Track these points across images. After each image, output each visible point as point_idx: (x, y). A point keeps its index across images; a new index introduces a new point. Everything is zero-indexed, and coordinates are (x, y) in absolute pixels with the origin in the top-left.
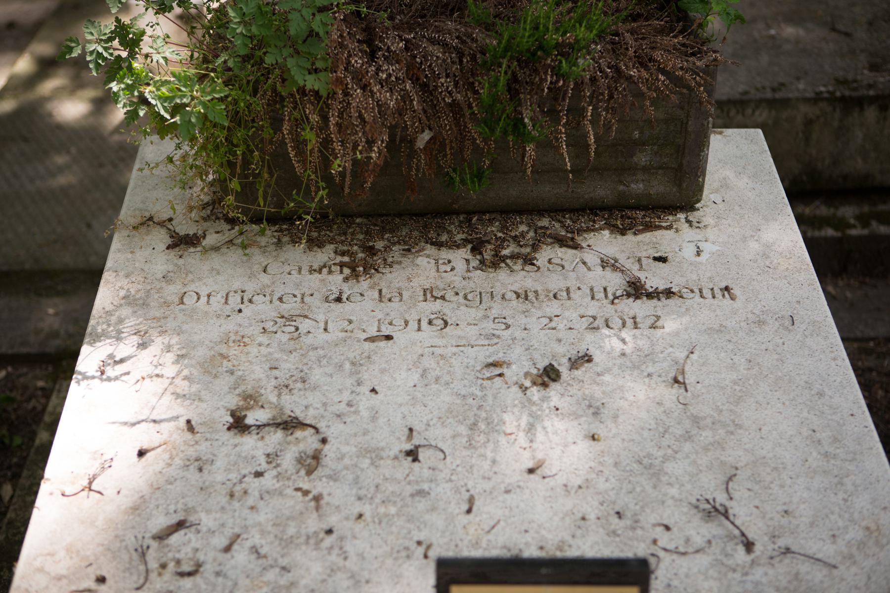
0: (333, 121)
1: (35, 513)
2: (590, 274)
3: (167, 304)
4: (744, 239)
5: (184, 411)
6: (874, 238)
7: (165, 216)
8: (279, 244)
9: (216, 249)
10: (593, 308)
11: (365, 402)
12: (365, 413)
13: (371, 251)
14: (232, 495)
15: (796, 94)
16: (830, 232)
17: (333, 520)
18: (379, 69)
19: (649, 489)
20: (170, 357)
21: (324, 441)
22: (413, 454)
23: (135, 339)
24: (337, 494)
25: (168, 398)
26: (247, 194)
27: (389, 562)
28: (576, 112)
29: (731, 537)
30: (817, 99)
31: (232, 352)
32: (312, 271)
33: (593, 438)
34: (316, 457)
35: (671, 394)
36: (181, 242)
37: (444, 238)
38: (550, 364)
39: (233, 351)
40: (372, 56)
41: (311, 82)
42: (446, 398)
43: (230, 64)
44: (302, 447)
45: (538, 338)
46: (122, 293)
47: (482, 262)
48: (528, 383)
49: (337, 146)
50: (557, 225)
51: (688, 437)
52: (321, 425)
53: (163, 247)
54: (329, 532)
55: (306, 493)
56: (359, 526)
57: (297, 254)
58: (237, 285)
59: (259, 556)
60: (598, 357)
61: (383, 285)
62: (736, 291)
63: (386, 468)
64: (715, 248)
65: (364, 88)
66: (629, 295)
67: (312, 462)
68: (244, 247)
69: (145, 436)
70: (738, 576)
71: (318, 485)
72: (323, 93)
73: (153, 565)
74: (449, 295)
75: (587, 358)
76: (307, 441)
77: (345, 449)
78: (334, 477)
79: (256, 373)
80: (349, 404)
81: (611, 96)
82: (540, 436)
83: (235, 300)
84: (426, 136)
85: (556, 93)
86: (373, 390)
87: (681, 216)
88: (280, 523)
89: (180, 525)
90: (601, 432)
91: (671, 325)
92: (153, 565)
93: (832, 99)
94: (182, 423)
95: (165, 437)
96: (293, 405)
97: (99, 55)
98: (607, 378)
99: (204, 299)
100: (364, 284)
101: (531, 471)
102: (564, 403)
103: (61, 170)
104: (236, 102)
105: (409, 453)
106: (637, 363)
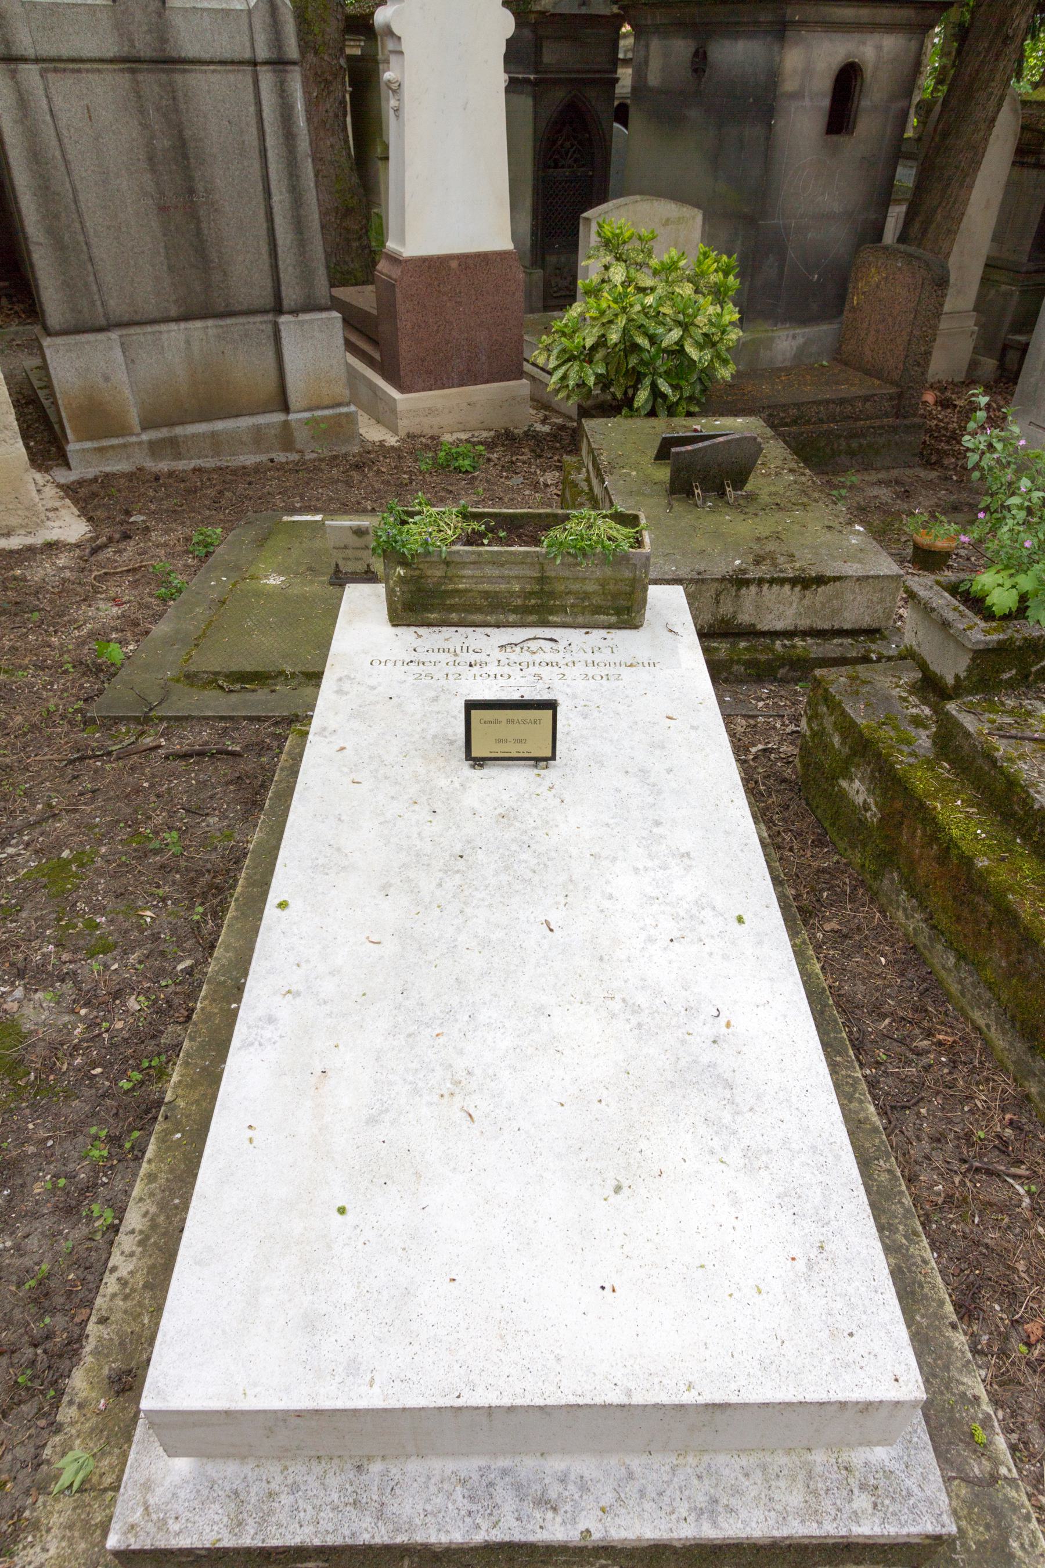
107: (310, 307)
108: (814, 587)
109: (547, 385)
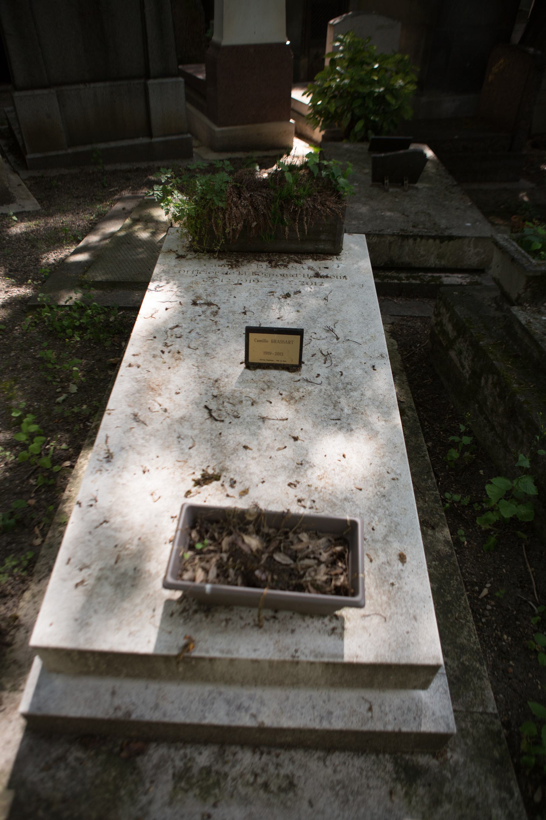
0: (227, 216)
1: (136, 322)
2: (304, 271)
3: (175, 273)
4: (353, 264)
5: (179, 300)
6: (411, 284)
7: (175, 250)
8: (210, 258)
9: (190, 259)
10: (303, 279)
11: (232, 300)
12: (232, 303)
13: (238, 261)
14: (192, 320)
15: (386, 233)
16: (396, 281)
17: (220, 327)
18: (241, 202)
19: (312, 324)
20: (175, 286)
21: (219, 308)
22: (245, 313)
23: (165, 282)
24: (222, 321)
25: (174, 297)
26: (200, 242)
27: (235, 338)
28: (301, 219)
29: (333, 336)
30: (393, 235)
31: (194, 286)
32: (219, 266)
33: (298, 311)
34: (217, 312)
35: (322, 303)
36: (180, 257)
37: (261, 259)
38: (303, 329)
39: (194, 286)
40: (240, 198)
41: (221, 205)
42: (256, 300)
43: (197, 199)
44: (212, 310)
45: (286, 286)
46: (162, 270)
47: (271, 266)
48: (281, 297)
49: (228, 225)
50: (296, 257)
51: (326, 313)
52: (219, 305)
53: (174, 258)
54: (219, 330)
55: (213, 321)
56: (227, 329)
57: (215, 261)
58: (196, 269)
59: (199, 334)
60: (303, 292)
61: (240, 270)
62: (348, 277)
63: (237, 316)
64: (343, 266)
65: (237, 207)
66: (315, 277)
67: (215, 314)
68: (199, 259)
69: (167, 305)
70: (333, 345)
71: (216, 319)
72: (224, 208)
73: (169, 335)
74: (260, 274)
75: (300, 292)
76: (214, 308)
77: (225, 311)
78: (221, 317)
79: (200, 291)
80: (227, 300)
81: (312, 214)
82: (282, 310)
83: (195, 273)
84: (255, 223)
85: (295, 212)
86: (235, 297)
87: (335, 257)
88: (205, 327)
89: (177, 326)
90: (301, 310)
91: (326, 285)
92: (169, 335)
93: (398, 235)
94: (178, 302)
95: (173, 306)
96: (211, 299)
97: (158, 195)
98: (304, 297)
99: (186, 272)
100: (235, 270)
101: (278, 318)
102: (290, 303)
103: (141, 253)
104: (198, 210)
105: (243, 313)
106: (314, 295)
107: (165, 74)
108: (446, 242)
109: (155, 199)
